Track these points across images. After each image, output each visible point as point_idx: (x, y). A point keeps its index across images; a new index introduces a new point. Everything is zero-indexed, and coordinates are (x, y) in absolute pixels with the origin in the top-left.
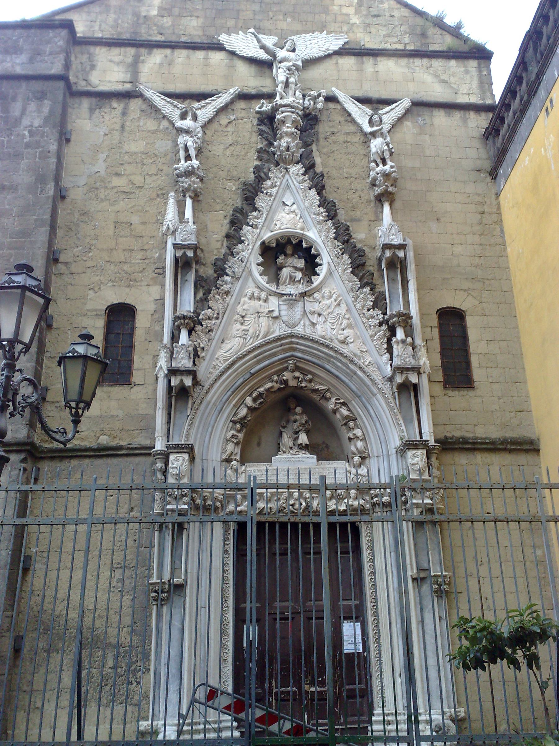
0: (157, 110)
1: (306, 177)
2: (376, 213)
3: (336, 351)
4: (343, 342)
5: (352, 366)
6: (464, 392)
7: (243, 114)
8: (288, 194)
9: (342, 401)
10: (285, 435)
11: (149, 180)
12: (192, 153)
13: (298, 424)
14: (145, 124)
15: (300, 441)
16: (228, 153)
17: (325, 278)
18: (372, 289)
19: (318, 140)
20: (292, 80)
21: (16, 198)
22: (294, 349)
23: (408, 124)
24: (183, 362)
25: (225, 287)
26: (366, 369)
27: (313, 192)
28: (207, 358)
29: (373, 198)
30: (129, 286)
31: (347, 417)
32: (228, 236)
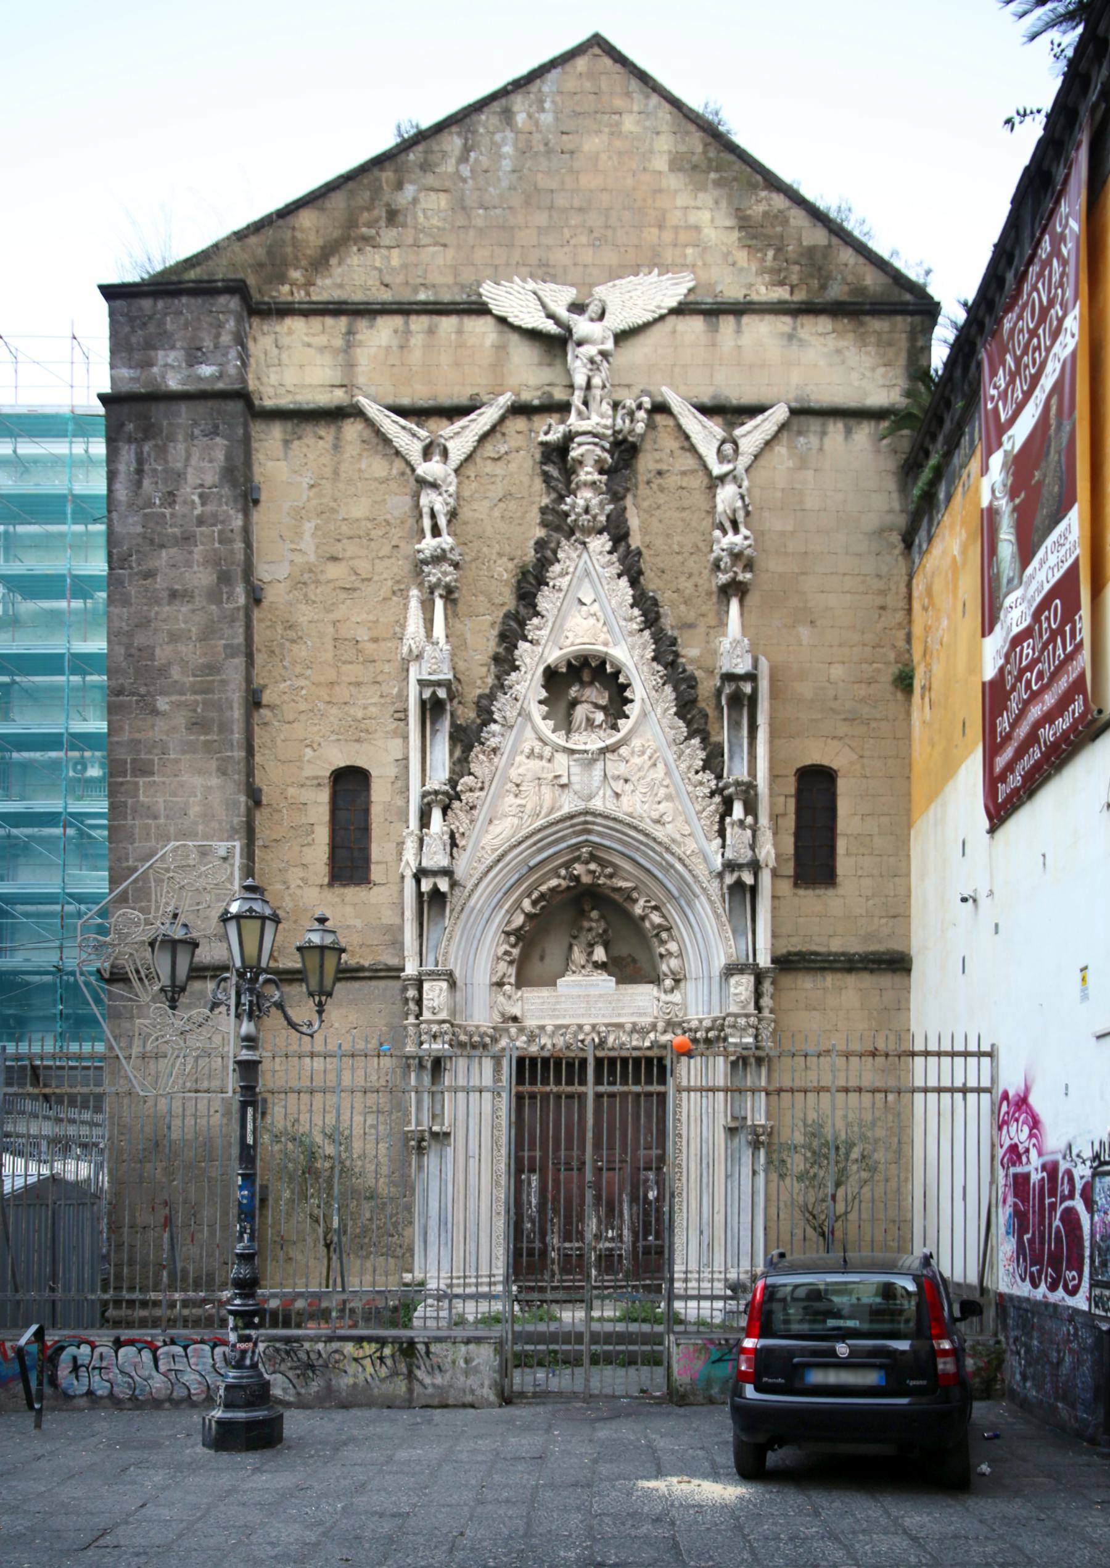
0: (386, 441)
1: (614, 557)
2: (718, 613)
3: (647, 835)
4: (657, 822)
5: (668, 856)
6: (820, 892)
8: (586, 583)
9: (653, 903)
10: (576, 949)
11: (379, 566)
12: (442, 522)
13: (594, 933)
14: (370, 466)
15: (595, 957)
16: (497, 513)
17: (637, 724)
18: (703, 741)
19: (636, 486)
20: (596, 381)
21: (193, 611)
22: (589, 832)
23: (781, 449)
24: (437, 858)
25: (493, 742)
26: (687, 861)
27: (624, 582)
28: (469, 848)
29: (715, 589)
30: (358, 741)
31: (660, 926)
32: (496, 659)
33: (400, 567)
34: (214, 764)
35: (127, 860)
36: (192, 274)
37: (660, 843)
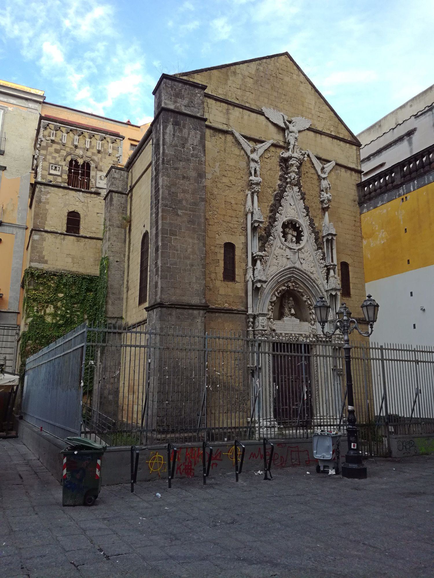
0: (239, 143)
7: (273, 154)
21: (190, 184)
22: (293, 273)
30: (232, 235)
33: (242, 183)
34: (196, 236)
35: (167, 264)
36: (185, 78)
37: (312, 280)
